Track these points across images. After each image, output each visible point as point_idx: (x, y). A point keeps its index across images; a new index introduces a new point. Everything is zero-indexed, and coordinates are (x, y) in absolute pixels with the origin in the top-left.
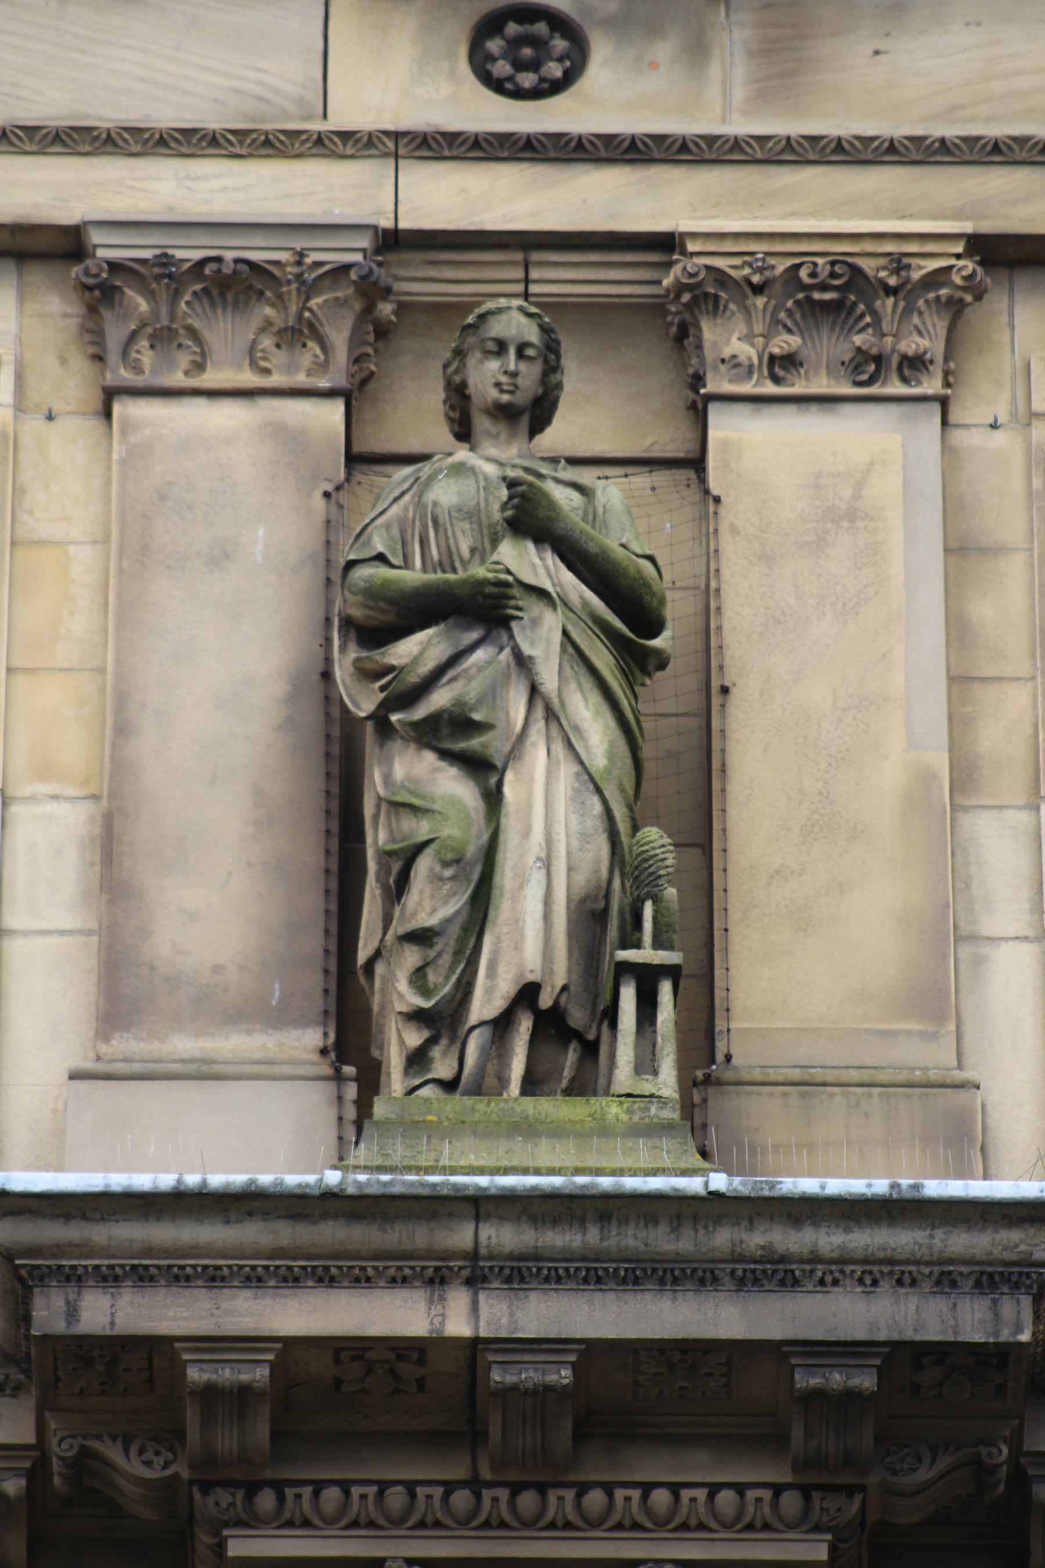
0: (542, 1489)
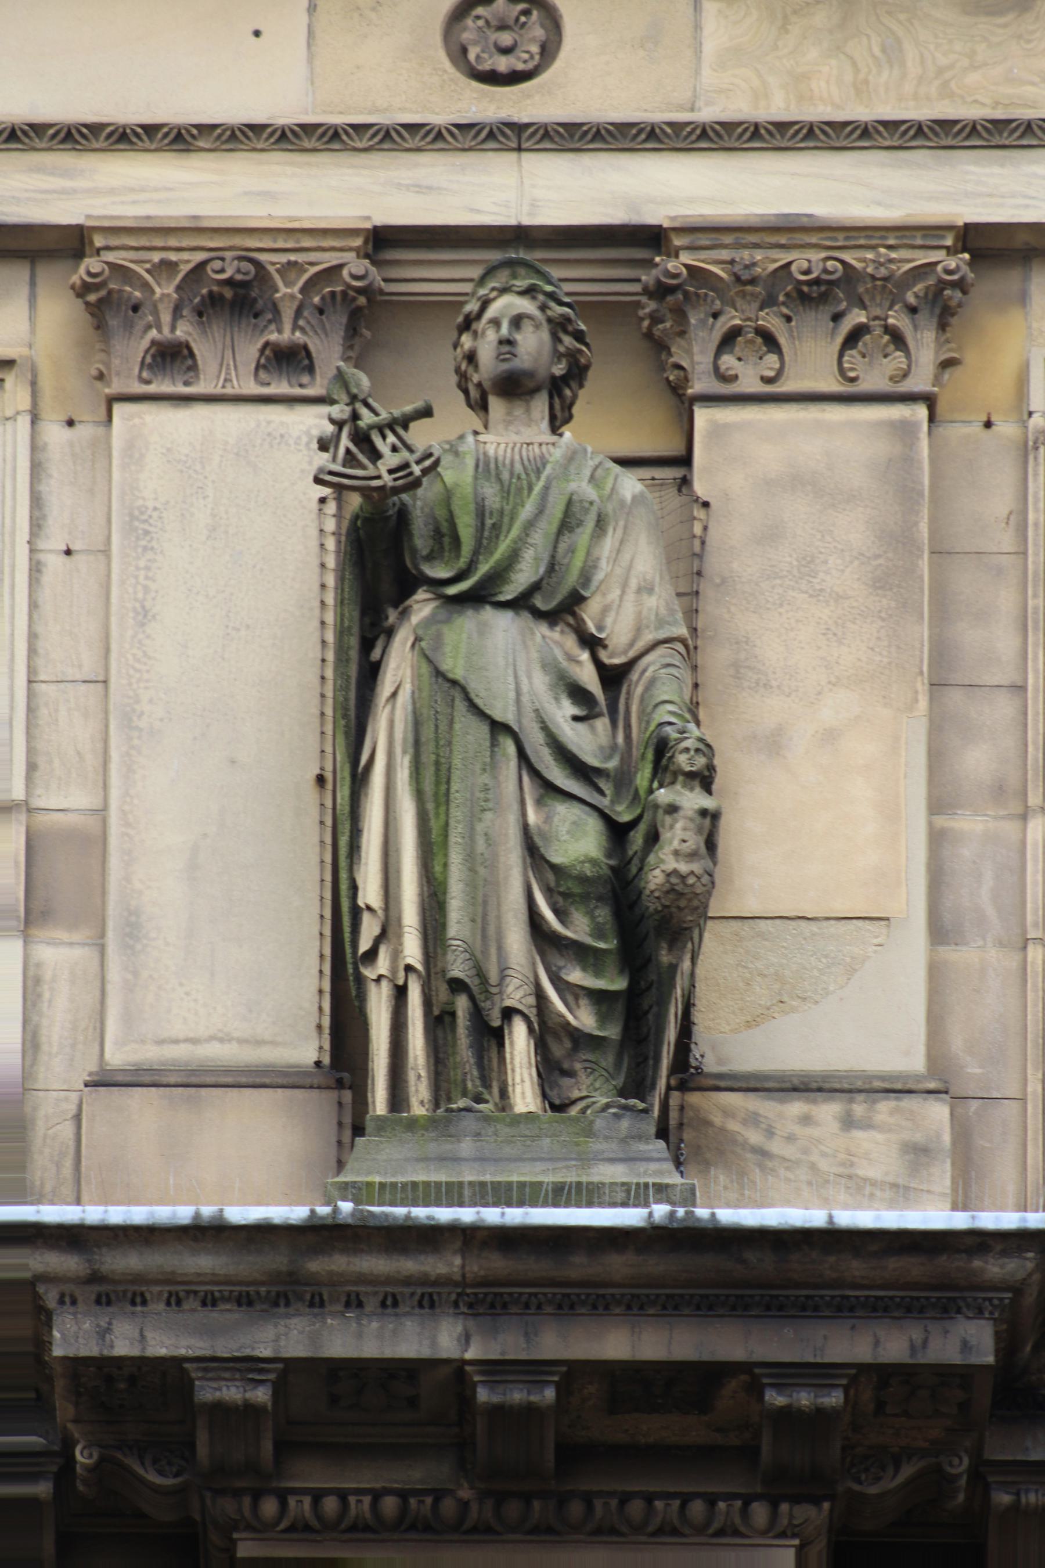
0: (527, 1498)
